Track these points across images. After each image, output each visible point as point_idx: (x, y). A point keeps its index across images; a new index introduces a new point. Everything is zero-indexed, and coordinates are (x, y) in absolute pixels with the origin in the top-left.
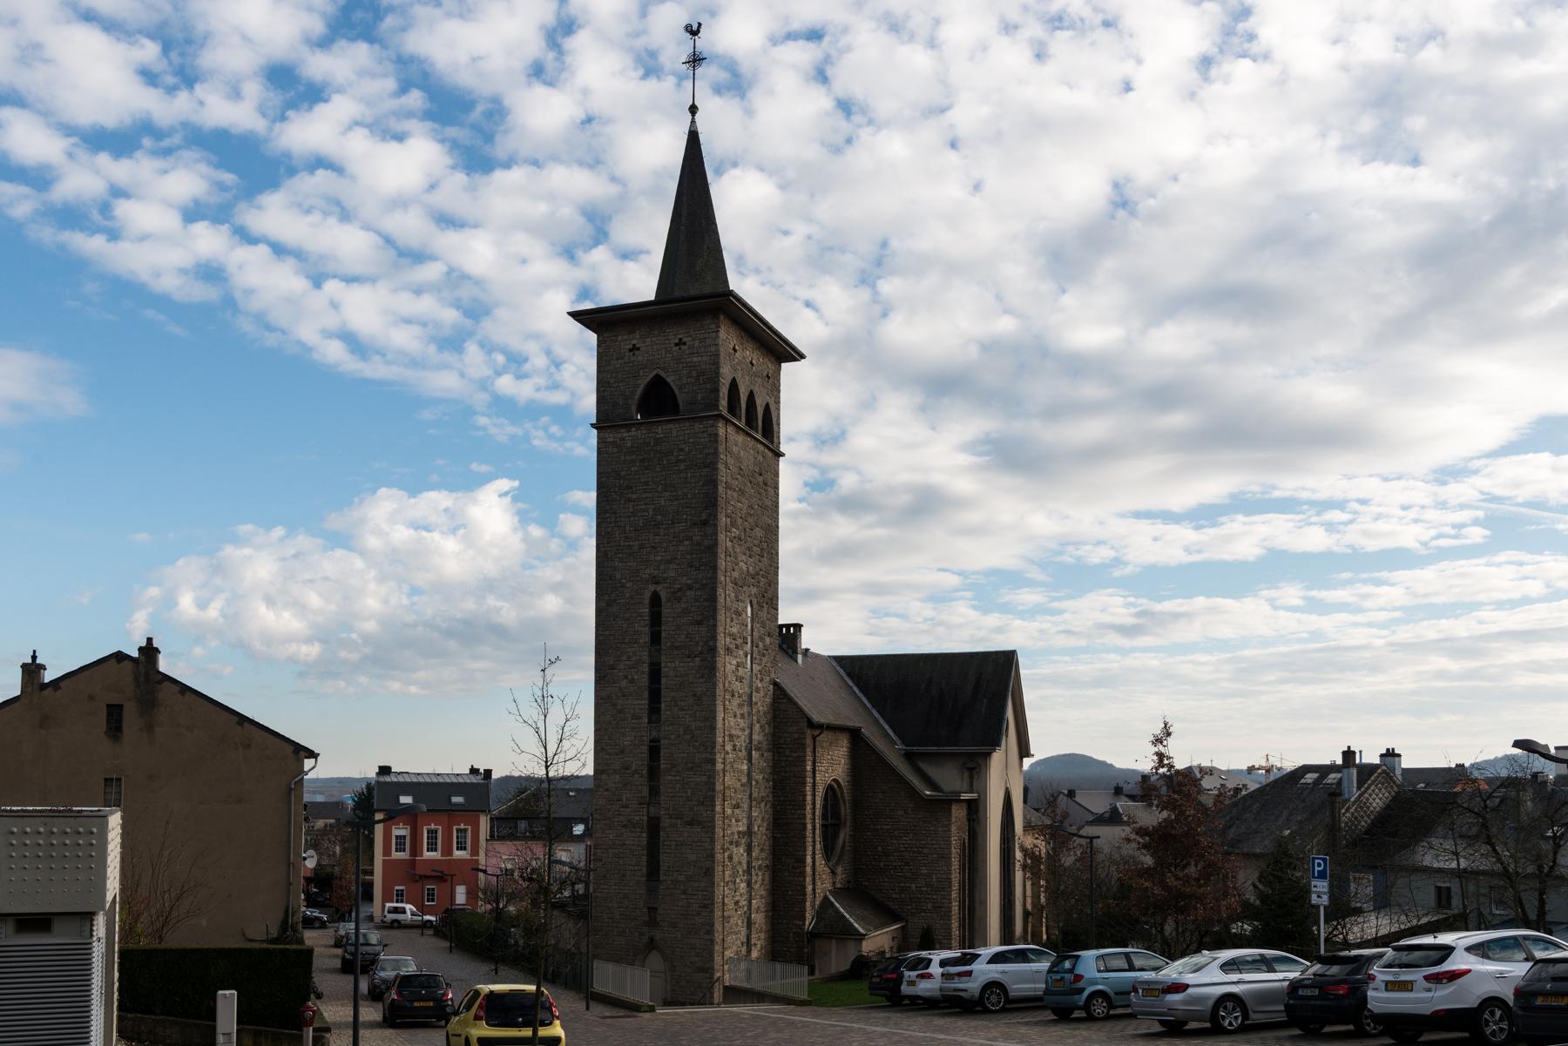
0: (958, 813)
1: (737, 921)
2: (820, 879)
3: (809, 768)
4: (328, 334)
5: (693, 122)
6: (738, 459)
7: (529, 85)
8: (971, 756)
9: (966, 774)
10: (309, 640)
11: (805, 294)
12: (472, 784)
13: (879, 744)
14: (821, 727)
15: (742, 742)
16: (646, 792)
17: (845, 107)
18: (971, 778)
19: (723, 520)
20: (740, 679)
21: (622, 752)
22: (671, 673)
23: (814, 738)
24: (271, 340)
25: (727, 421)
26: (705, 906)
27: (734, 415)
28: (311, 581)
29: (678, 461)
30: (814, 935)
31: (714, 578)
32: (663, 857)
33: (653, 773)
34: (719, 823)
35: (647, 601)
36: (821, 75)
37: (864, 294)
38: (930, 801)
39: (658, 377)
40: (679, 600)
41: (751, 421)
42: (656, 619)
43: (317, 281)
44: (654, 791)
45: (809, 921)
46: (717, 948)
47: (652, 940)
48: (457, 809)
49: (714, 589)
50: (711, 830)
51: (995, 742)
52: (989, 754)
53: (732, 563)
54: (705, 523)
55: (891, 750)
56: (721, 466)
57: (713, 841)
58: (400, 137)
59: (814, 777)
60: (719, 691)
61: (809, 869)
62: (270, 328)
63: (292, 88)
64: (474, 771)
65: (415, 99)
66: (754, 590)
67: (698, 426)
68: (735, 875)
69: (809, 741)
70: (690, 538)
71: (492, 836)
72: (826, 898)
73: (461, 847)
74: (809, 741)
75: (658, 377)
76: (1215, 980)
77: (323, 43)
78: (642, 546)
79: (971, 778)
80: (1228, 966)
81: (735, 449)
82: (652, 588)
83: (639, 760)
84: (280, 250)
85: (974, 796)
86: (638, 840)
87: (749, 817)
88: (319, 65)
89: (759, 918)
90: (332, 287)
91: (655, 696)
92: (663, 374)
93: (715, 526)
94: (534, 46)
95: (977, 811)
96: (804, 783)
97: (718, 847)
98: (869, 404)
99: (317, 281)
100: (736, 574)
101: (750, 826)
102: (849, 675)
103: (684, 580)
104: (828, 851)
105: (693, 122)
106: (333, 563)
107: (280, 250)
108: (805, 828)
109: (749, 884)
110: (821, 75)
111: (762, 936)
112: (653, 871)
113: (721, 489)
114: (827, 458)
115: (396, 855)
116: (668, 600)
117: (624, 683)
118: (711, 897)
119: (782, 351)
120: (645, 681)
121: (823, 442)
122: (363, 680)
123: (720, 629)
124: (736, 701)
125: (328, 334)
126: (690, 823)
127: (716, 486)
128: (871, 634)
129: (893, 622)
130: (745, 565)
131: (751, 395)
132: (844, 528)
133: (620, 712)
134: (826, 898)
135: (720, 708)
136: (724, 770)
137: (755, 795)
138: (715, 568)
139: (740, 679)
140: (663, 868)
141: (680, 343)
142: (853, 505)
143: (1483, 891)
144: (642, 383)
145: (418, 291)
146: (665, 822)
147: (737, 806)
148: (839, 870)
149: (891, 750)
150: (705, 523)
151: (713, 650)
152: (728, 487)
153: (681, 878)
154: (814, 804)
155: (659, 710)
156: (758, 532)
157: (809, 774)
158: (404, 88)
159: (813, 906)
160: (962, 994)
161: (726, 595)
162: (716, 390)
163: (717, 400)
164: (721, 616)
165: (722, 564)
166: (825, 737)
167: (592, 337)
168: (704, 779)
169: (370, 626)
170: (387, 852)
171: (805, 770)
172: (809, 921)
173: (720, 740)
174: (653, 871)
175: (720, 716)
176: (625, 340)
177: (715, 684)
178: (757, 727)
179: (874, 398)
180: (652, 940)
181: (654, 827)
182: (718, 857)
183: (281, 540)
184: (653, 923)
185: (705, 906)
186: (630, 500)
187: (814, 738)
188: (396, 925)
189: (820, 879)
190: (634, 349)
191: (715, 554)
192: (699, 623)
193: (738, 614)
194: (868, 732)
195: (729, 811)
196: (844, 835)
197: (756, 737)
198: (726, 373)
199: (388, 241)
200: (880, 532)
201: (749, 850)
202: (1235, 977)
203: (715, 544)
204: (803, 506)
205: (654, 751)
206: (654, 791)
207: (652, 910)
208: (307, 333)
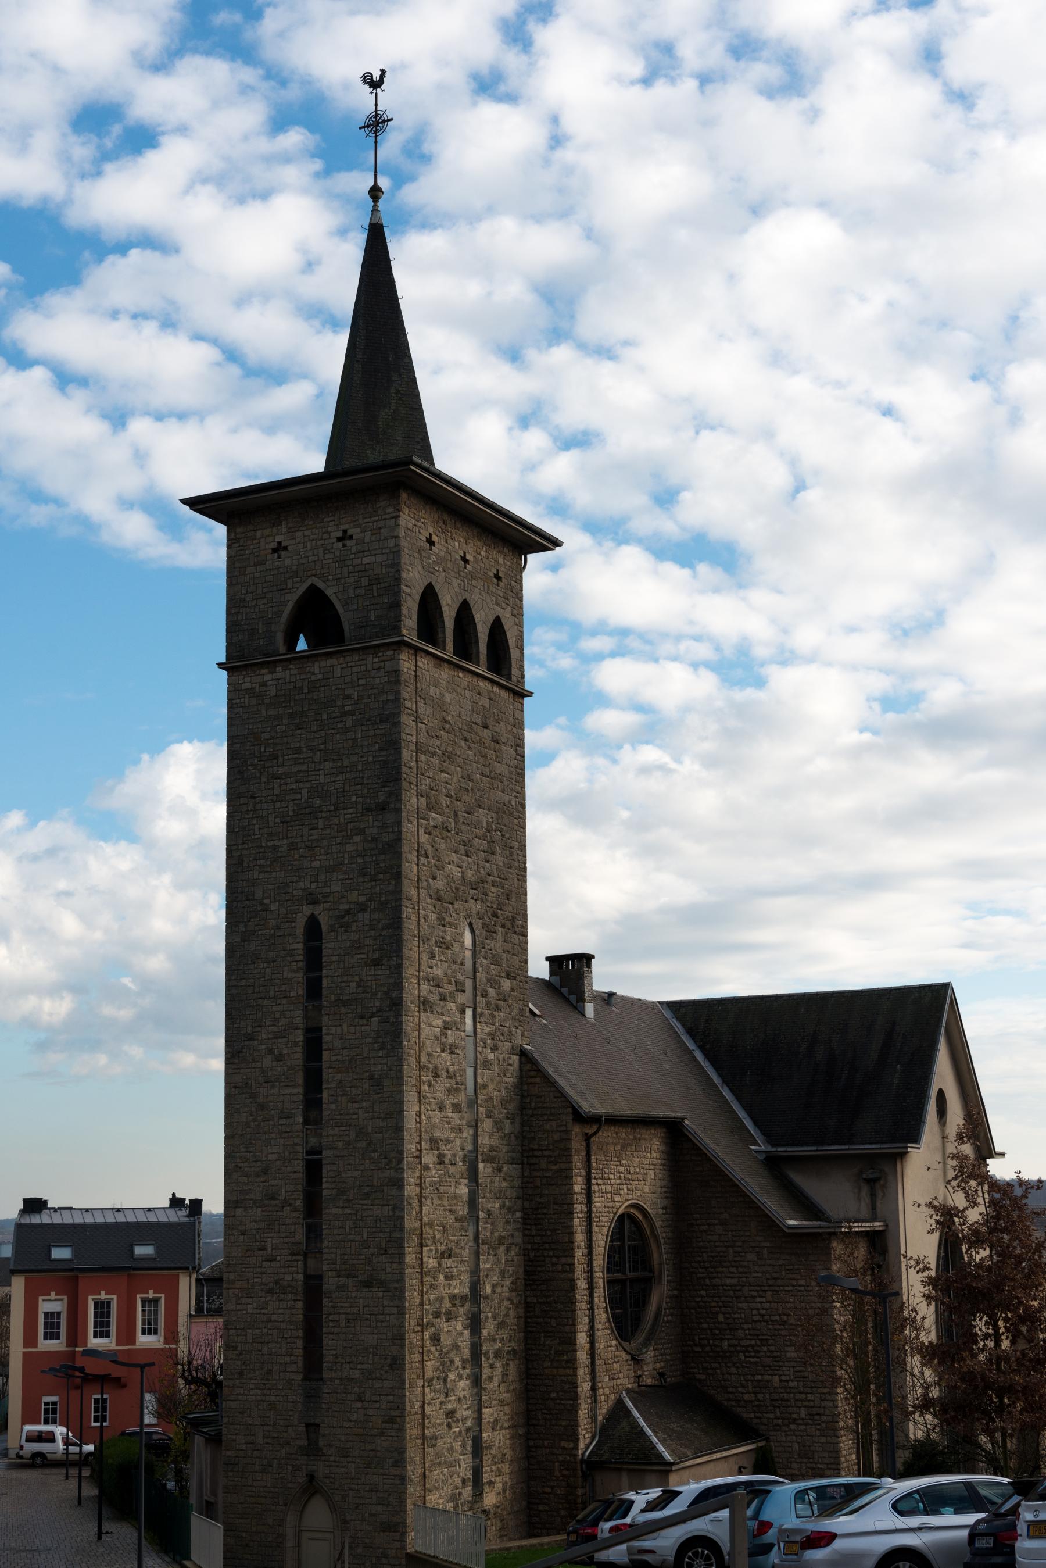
0: (844, 1261)
1: (452, 1444)
2: (606, 1370)
3: (578, 1188)
4: (126, 504)
5: (375, 210)
6: (440, 705)
7: (475, 104)
8: (871, 1159)
9: (865, 1190)
10: (54, 991)
11: (886, 393)
12: (169, 1225)
13: (715, 1143)
14: (595, 1120)
15: (458, 1145)
16: (300, 1235)
17: (962, 98)
18: (873, 1195)
19: (411, 801)
20: (452, 1050)
21: (265, 1171)
22: (337, 1044)
23: (587, 1138)
24: (39, 515)
25: (417, 650)
26: (391, 1420)
27: (434, 643)
28: (68, 894)
29: (345, 714)
30: (593, 1466)
31: (398, 891)
32: (328, 1341)
33: (313, 1205)
34: (411, 1281)
35: (300, 930)
36: (930, 57)
37: (981, 392)
38: (797, 1237)
39: (313, 588)
40: (346, 927)
41: (465, 646)
42: (314, 959)
43: (118, 418)
44: (313, 1233)
45: (585, 1443)
46: (412, 1490)
47: (311, 1477)
48: (146, 1266)
49: (398, 909)
50: (398, 1293)
51: (914, 1136)
52: (903, 1155)
53: (431, 862)
54: (383, 808)
55: (736, 1153)
56: (405, 719)
57: (401, 1312)
58: (265, 195)
59: (589, 1202)
60: (410, 1066)
61: (582, 1356)
62: (38, 496)
63: (109, 130)
64: (176, 1202)
65: (294, 138)
66: (477, 907)
67: (371, 660)
68: (445, 1365)
69: (577, 1144)
70: (361, 832)
71: (199, 1310)
72: (620, 1402)
73: (102, 1332)
74: (577, 1144)
75: (313, 588)
76: (881, 1526)
77: (162, 64)
78: (293, 847)
79: (873, 1195)
80: (900, 1507)
81: (433, 691)
82: (307, 910)
83: (290, 1182)
84: (66, 379)
85: (878, 1225)
86: (290, 1312)
87: (475, 1272)
88: (157, 97)
89: (498, 1440)
90: (140, 428)
91: (313, 1081)
92: (321, 585)
93: (398, 811)
94: (486, 48)
95: (884, 1251)
96: (570, 1213)
97: (411, 1322)
98: (982, 569)
99: (118, 418)
100: (439, 884)
101: (475, 1287)
102: (691, 1032)
103: (354, 896)
104: (625, 1325)
105: (375, 210)
106: (110, 863)
107: (66, 379)
108: (573, 1287)
109: (476, 1381)
110: (930, 57)
111: (506, 1468)
112: (313, 1366)
113: (406, 754)
114: (914, 658)
115: (45, 1345)
116: (332, 929)
117: (267, 1062)
118: (400, 1406)
119: (520, 540)
120: (298, 1057)
121: (906, 633)
122: (136, 1051)
123: (409, 971)
124: (443, 1084)
125: (126, 504)
126: (368, 1284)
127: (398, 751)
128: (966, 946)
129: (1002, 924)
130: (455, 867)
131: (464, 612)
132: (932, 772)
133: (262, 1107)
134: (620, 1402)
135: (410, 1097)
136: (421, 1197)
137: (485, 1234)
138: (398, 877)
139: (452, 1050)
140: (328, 1358)
141: (344, 537)
142: (952, 731)
143: (718, 1371)
144: (292, 599)
145: (272, 427)
146: (330, 1283)
147: (449, 1254)
148: (649, 1355)
149: (736, 1153)
150: (383, 808)
151: (397, 1005)
152: (420, 749)
153: (356, 1374)
154: (590, 1247)
155: (318, 1103)
156: (483, 816)
157: (582, 1198)
158: (280, 122)
159: (593, 1418)
160: (648, 1558)
161: (418, 916)
162: (396, 605)
163: (398, 619)
164: (411, 951)
165: (410, 868)
166: (606, 1135)
167: (220, 530)
168: (387, 1211)
169: (156, 964)
170: (30, 1339)
171: (570, 1193)
172: (585, 1443)
173: (411, 1147)
174: (313, 1366)
175: (411, 1110)
176: (267, 536)
177: (400, 1060)
178: (487, 1125)
179: (992, 556)
180: (311, 1477)
181: (313, 1290)
182: (412, 1338)
183: (19, 831)
184: (312, 1450)
185: (391, 1420)
186: (276, 777)
187: (587, 1138)
188: (39, 1461)
189: (606, 1370)
190: (344, 537)
191: (398, 855)
192: (376, 963)
193: (444, 945)
194: (701, 1126)
195: (431, 1263)
196: (659, 1297)
197: (484, 1141)
198: (414, 579)
199: (231, 355)
200: (996, 776)
201: (475, 1324)
202: (914, 1521)
203: (399, 840)
204: (867, 736)
205: (313, 1169)
206: (313, 1233)
207: (312, 1428)
208: (96, 503)
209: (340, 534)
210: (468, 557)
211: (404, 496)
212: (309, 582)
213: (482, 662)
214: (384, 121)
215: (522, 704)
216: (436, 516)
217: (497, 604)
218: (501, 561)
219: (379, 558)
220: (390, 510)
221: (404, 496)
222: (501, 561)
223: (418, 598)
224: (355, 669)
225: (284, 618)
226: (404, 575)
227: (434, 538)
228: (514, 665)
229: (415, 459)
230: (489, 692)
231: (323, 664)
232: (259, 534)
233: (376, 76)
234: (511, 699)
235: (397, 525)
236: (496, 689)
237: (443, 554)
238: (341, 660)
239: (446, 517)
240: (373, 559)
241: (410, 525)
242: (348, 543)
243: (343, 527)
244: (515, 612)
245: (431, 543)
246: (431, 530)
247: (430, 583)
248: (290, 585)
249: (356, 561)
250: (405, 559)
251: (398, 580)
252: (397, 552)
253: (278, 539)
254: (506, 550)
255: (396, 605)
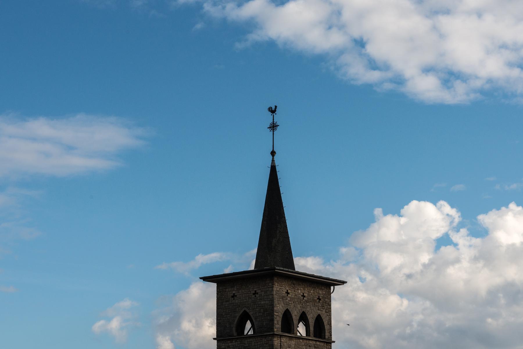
5: (273, 160)
92: (248, 311)
105: (273, 160)
141: (255, 293)
163: (273, 325)
209: (254, 292)
210: (305, 295)
211: (275, 279)
212: (244, 310)
213: (311, 334)
214: (276, 126)
215: (331, 346)
216: (290, 283)
217: (319, 310)
218: (320, 292)
219: (267, 302)
220: (270, 284)
221: (275, 279)
222: (321, 292)
223: (281, 316)
224: (259, 343)
225: (235, 323)
226: (275, 309)
227: (289, 291)
228: (326, 331)
229: (277, 268)
230: (314, 345)
231: (248, 340)
232: (227, 290)
233: (273, 108)
234: (325, 345)
235: (273, 290)
236: (318, 343)
237: (293, 296)
238: (254, 339)
239: (294, 282)
240: (264, 302)
241: (278, 289)
242: (257, 296)
243: (255, 290)
244: (327, 311)
245: (288, 293)
246: (287, 289)
247: (287, 309)
248: (237, 310)
249: (259, 303)
250: (276, 302)
251: (273, 311)
252: (272, 300)
253: (234, 292)
254: (323, 288)
255: (272, 320)
